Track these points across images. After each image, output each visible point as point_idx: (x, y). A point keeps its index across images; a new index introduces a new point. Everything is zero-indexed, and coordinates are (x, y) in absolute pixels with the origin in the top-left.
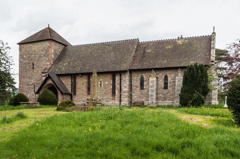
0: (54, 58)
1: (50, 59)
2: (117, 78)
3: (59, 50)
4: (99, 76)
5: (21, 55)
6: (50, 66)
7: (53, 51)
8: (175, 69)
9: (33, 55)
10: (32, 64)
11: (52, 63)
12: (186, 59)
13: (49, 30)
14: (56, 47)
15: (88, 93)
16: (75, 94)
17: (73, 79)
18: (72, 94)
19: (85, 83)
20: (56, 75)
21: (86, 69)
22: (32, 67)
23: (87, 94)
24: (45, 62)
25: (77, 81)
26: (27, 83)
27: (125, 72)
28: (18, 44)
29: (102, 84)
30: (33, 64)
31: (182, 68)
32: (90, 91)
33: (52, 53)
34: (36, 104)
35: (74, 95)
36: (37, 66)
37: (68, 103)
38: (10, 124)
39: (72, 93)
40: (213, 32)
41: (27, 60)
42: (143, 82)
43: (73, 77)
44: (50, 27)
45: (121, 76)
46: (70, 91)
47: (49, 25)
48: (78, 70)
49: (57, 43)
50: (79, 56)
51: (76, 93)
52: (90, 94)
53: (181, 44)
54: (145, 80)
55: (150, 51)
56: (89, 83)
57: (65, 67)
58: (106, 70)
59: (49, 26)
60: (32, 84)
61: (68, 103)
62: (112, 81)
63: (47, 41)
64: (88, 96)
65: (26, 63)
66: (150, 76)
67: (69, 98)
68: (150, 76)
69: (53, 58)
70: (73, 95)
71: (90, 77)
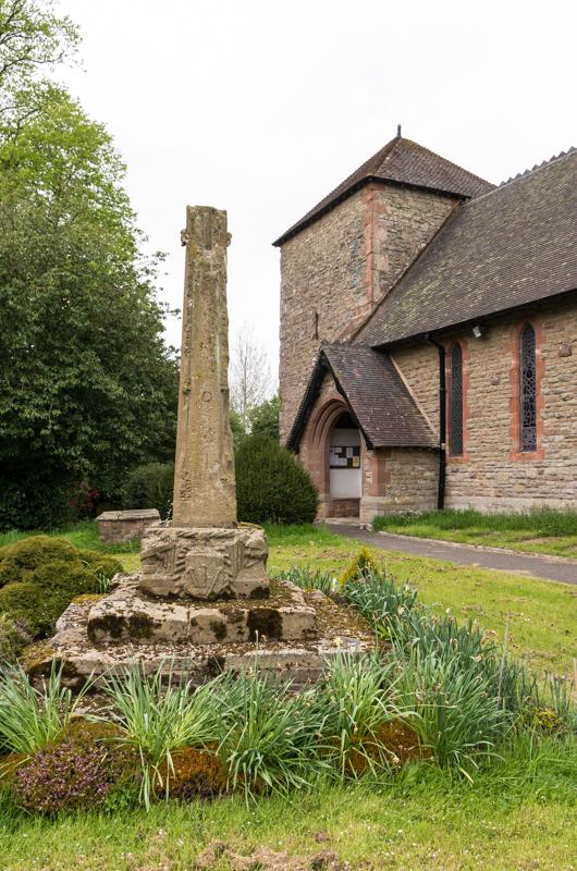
0: (387, 269)
3: (425, 227)
6: (369, 312)
7: (382, 235)
9: (317, 278)
11: (379, 295)
14: (400, 212)
16: (458, 449)
17: (448, 360)
18: (446, 447)
21: (515, 288)
22: (314, 332)
23: (516, 444)
24: (352, 296)
25: (464, 369)
28: (275, 244)
32: (534, 425)
33: (378, 248)
34: (139, 525)
39: (443, 440)
43: (447, 348)
44: (403, 136)
46: (432, 422)
47: (399, 128)
48: (471, 308)
50: (502, 230)
52: (534, 448)
56: (528, 376)
59: (399, 134)
64: (524, 460)
67: (428, 474)
69: (382, 273)
70: (447, 452)
71: (533, 332)
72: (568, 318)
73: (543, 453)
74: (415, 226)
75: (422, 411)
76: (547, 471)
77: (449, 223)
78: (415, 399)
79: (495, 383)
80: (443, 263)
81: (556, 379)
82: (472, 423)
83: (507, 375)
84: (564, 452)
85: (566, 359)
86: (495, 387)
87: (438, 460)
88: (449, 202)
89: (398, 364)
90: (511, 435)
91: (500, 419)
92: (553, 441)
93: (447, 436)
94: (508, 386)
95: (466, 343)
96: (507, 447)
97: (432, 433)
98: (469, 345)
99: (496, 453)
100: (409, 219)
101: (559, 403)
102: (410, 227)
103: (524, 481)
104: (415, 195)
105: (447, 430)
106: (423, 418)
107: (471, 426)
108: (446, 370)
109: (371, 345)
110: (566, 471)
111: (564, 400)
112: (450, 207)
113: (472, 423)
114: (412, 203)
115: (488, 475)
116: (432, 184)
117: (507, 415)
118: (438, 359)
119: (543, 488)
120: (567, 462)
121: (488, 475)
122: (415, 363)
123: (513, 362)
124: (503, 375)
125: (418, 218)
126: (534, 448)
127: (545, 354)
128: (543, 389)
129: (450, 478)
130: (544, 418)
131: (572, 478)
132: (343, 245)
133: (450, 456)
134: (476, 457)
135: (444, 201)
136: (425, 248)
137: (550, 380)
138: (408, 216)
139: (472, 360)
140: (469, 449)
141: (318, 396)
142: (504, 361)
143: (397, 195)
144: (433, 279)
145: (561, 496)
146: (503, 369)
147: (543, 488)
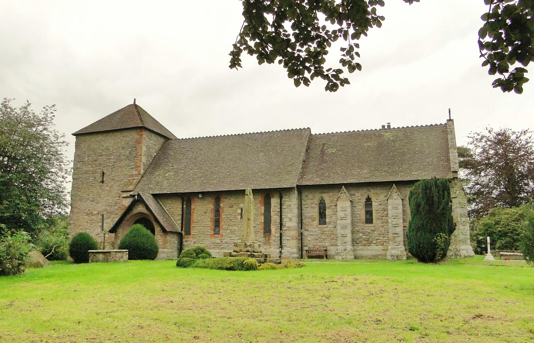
2: (275, 202)
10: (102, 172)
11: (142, 172)
15: (215, 230)
16: (188, 233)
17: (185, 203)
18: (183, 232)
19: (209, 211)
20: (152, 194)
22: (101, 180)
23: (212, 233)
24: (128, 169)
25: (192, 207)
26: (87, 211)
27: (289, 190)
28: (74, 135)
30: (103, 173)
31: (400, 184)
36: (112, 178)
39: (182, 230)
44: (137, 103)
45: (281, 198)
47: (135, 100)
52: (219, 234)
54: (327, 205)
55: (334, 152)
56: (217, 212)
60: (98, 214)
62: (263, 207)
68: (339, 197)
69: (144, 163)
70: (184, 234)
72: (235, 198)
73: (222, 236)
75: (172, 219)
78: (169, 215)
80: (171, 165)
82: (195, 225)
83: (210, 211)
84: (230, 235)
85: (231, 208)
86: (205, 214)
87: (180, 237)
88: (163, 139)
89: (161, 201)
90: (210, 230)
91: (207, 224)
93: (184, 229)
95: (193, 198)
96: (209, 233)
100: (152, 144)
101: (228, 221)
103: (215, 244)
104: (154, 135)
105: (184, 227)
106: (173, 222)
107: (195, 226)
110: (231, 241)
111: (230, 220)
112: (163, 141)
113: (195, 225)
114: (153, 138)
115: (201, 242)
117: (210, 223)
119: (223, 246)
120: (231, 238)
121: (201, 242)
122: (169, 202)
123: (212, 207)
124: (208, 211)
128: (223, 216)
129: (185, 243)
130: (223, 224)
131: (232, 243)
134: (197, 236)
140: (193, 234)
142: (209, 206)
145: (228, 248)
146: (209, 209)
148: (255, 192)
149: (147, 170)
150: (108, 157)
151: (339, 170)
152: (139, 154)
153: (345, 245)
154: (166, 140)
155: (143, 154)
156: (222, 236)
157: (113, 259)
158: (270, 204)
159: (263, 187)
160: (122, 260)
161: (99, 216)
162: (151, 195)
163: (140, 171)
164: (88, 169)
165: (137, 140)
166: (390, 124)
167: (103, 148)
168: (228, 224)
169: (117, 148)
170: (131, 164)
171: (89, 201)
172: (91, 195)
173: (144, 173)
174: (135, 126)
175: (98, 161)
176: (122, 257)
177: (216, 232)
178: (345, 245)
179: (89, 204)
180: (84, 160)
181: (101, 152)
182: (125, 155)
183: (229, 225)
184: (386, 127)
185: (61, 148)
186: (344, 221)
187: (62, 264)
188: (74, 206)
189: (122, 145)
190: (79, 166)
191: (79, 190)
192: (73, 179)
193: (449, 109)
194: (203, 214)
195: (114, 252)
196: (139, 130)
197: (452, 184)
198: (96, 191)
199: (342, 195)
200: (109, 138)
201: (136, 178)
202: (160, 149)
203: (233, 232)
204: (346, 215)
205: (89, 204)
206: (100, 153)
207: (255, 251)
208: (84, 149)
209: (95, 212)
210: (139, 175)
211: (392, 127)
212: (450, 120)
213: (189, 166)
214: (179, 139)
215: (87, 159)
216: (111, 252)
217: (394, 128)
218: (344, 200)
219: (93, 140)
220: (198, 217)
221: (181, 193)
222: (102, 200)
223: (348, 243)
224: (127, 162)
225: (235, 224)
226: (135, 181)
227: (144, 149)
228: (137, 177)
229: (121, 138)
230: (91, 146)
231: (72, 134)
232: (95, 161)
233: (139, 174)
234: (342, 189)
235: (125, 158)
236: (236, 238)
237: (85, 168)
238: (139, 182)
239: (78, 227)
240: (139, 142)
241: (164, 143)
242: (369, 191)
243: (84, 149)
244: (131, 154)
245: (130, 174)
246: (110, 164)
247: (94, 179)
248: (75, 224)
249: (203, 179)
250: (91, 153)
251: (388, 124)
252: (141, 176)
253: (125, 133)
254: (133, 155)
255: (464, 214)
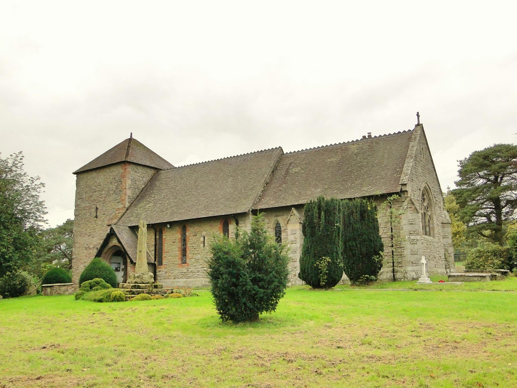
0: (131, 195)
1: (123, 198)
2: (232, 227)
3: (144, 179)
4: (149, 232)
5: (78, 193)
8: (287, 209)
9: (97, 193)
10: (96, 208)
11: (127, 205)
12: (357, 182)
13: (131, 142)
14: (136, 174)
15: (182, 260)
16: (161, 263)
17: (157, 233)
18: (156, 263)
19: (177, 241)
20: (129, 227)
22: (95, 215)
23: (180, 262)
25: (164, 237)
26: (85, 245)
27: (244, 215)
28: (74, 173)
29: (206, 240)
30: (97, 208)
31: (299, 207)
32: (186, 256)
35: (159, 265)
36: (103, 213)
37: (94, 283)
38: (478, 381)
39: (155, 260)
40: (417, 123)
41: (87, 203)
42: (281, 234)
43: (158, 229)
44: (133, 137)
45: (237, 224)
47: (131, 134)
49: (139, 167)
50: (174, 189)
51: (162, 261)
52: (186, 263)
53: (356, 151)
54: (282, 229)
55: (297, 171)
56: (184, 241)
57: (146, 211)
58: (211, 214)
60: (94, 247)
61: (94, 283)
63: (120, 165)
65: (85, 207)
66: (289, 220)
68: (289, 220)
69: (129, 196)
70: (157, 265)
71: (162, 233)
74: (141, 179)
76: (190, 270)
77: (152, 180)
79: (174, 242)
80: (153, 196)
81: (192, 243)
85: (195, 237)
86: (174, 244)
87: (153, 267)
92: (191, 261)
93: (157, 259)
94: (178, 244)
95: (164, 228)
97: (151, 258)
98: (165, 229)
99: (174, 265)
100: (139, 176)
102: (139, 179)
103: (182, 273)
105: (157, 257)
107: (166, 256)
108: (157, 237)
109: (129, 226)
110: (195, 270)
112: (153, 172)
114: (140, 170)
115: (171, 272)
116: (148, 164)
118: (154, 233)
119: (188, 275)
120: (196, 267)
121: (171, 272)
125: (142, 176)
126: (186, 263)
127: (189, 235)
128: (189, 245)
132: (111, 183)
133: (158, 266)
135: (151, 170)
136: (144, 187)
137: (191, 242)
138: (139, 175)
139: (166, 234)
141: (108, 243)
142: (177, 236)
143: (134, 167)
144: (150, 202)
147: (188, 275)
148: (150, 227)
149: (133, 202)
150: (100, 193)
151: (295, 190)
152: (124, 188)
153: (295, 270)
154: (157, 171)
155: (127, 187)
156: (188, 265)
157: (57, 292)
158: (228, 230)
159: (220, 214)
160: (67, 293)
161: (95, 249)
162: (128, 227)
163: (125, 204)
164: (85, 205)
165: (122, 174)
166: (371, 134)
167: (97, 185)
168: (193, 253)
169: (107, 183)
170: (117, 198)
171: (86, 236)
172: (88, 231)
173: (130, 206)
174: (101, 166)
175: (93, 198)
176: (67, 290)
177: (184, 262)
178: (295, 270)
179: (87, 239)
180: (83, 197)
181: (95, 188)
182: (113, 190)
183: (193, 254)
184: (367, 137)
185: (40, 189)
186: (294, 244)
187: (26, 299)
188: (76, 241)
189: (111, 180)
190: (79, 202)
191: (79, 225)
192: (75, 215)
193: (418, 113)
194: (173, 244)
195: (58, 285)
196: (123, 165)
197: (402, 198)
198: (92, 226)
199: (292, 217)
200: (101, 174)
201: (122, 211)
202: (150, 181)
203: (197, 260)
204: (296, 239)
205: (87, 239)
206: (95, 189)
207: (144, 282)
208: (83, 187)
209: (92, 246)
210: (124, 208)
211: (373, 136)
212: (418, 125)
213: (167, 196)
214: (176, 168)
215: (84, 196)
216: (54, 286)
217: (375, 137)
218: (294, 223)
219: (89, 177)
220: (168, 247)
221: (152, 224)
222: (97, 234)
223: (297, 268)
224: (114, 196)
225: (198, 252)
226: (120, 214)
227: (129, 182)
228: (123, 210)
229: (110, 174)
230: (88, 183)
231: (73, 173)
232: (91, 197)
233: (124, 207)
234: (291, 211)
235: (112, 193)
236: (200, 267)
237: (83, 205)
238: (123, 215)
239: (80, 261)
240: (123, 176)
241: (155, 174)
242: (277, 216)
243: (83, 187)
244: (117, 189)
245: (118, 207)
246: (102, 200)
247: (90, 215)
248: (77, 258)
249: (174, 208)
250: (88, 190)
251: (368, 134)
252: (126, 209)
253: (113, 169)
254: (119, 189)
255: (414, 231)
